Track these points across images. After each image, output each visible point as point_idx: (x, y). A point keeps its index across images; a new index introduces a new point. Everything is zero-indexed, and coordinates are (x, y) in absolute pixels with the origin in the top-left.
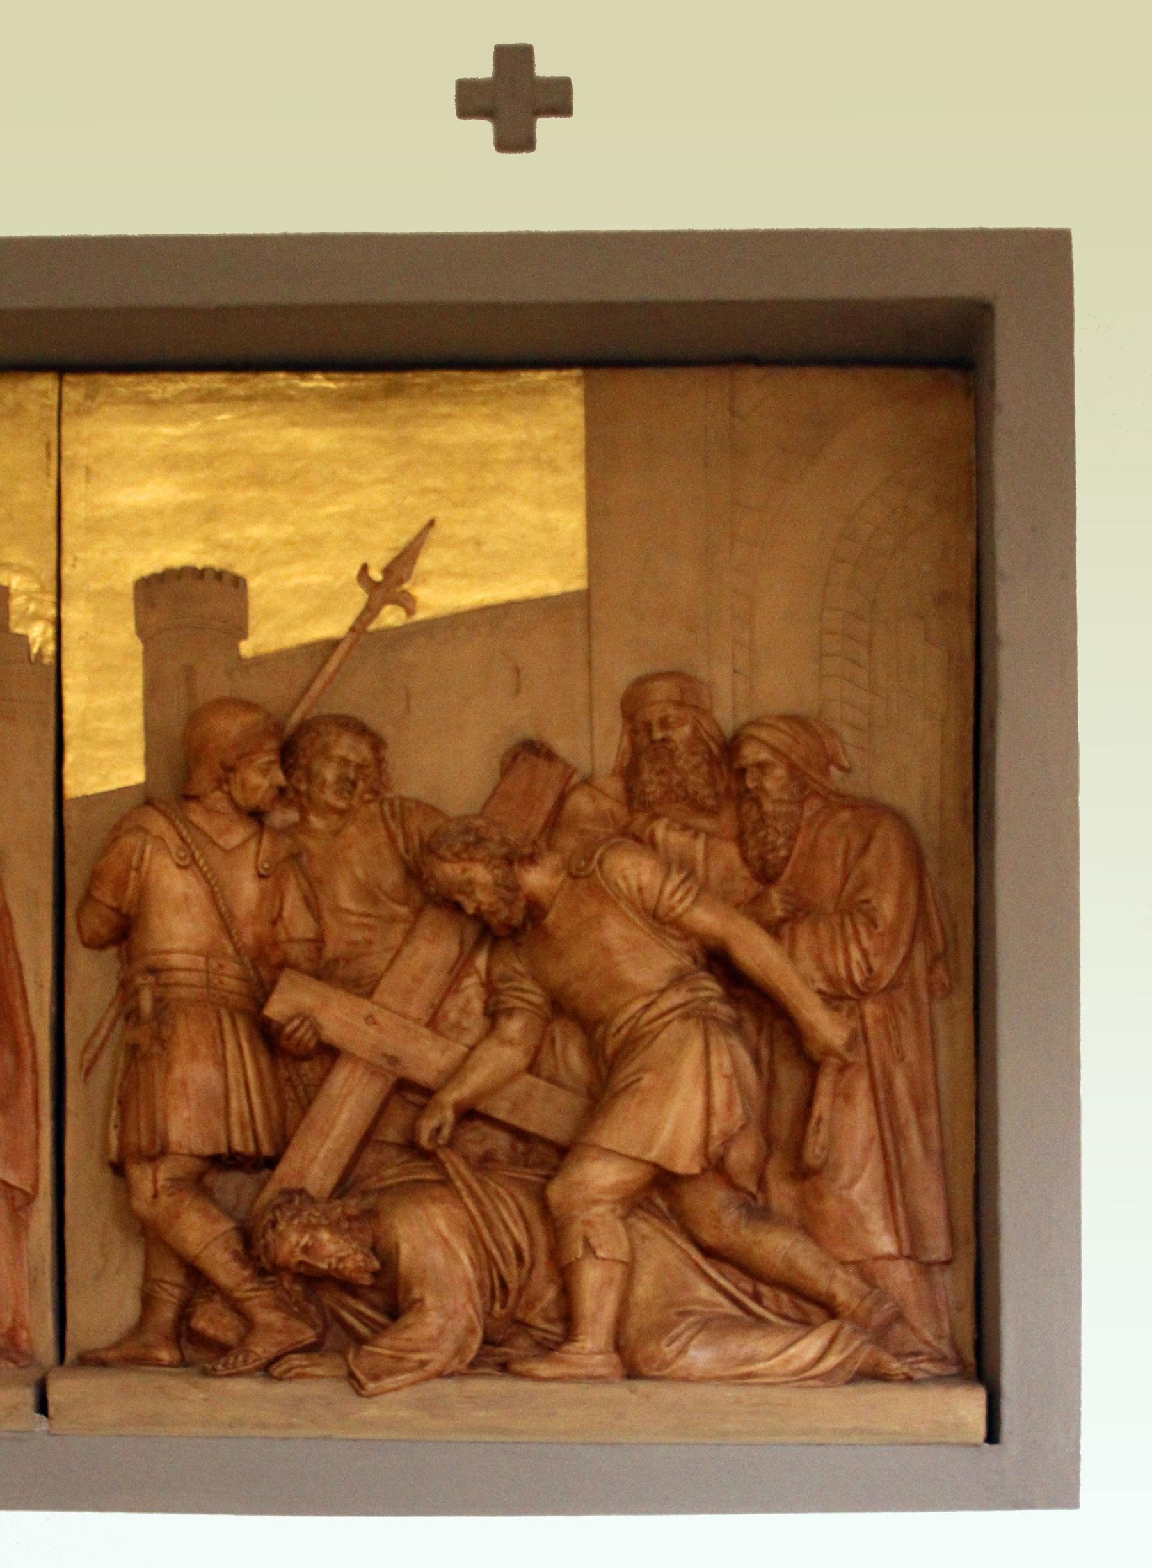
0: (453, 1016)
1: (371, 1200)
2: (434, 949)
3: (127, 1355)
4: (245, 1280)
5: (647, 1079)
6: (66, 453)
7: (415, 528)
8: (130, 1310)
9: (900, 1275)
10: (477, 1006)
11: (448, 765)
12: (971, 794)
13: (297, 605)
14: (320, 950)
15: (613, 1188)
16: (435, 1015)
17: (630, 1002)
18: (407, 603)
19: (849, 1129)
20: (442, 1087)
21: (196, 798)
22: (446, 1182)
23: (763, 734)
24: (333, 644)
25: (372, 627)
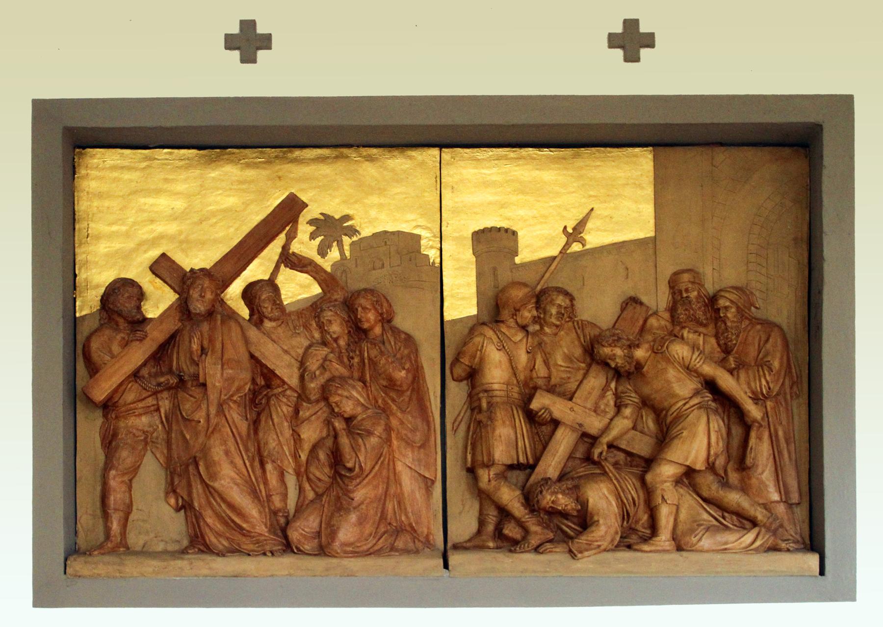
0: (602, 407)
1: (576, 482)
2: (596, 381)
3: (474, 544)
4: (526, 514)
5: (685, 433)
7: (586, 211)
8: (474, 526)
9: (781, 509)
10: (612, 403)
11: (599, 307)
12: (807, 319)
13: (537, 243)
14: (549, 381)
15: (673, 475)
16: (596, 407)
17: (677, 402)
18: (583, 242)
19: (761, 450)
20: (601, 436)
21: (502, 322)
22: (605, 473)
23: (727, 295)
24: (554, 258)
25: (568, 251)
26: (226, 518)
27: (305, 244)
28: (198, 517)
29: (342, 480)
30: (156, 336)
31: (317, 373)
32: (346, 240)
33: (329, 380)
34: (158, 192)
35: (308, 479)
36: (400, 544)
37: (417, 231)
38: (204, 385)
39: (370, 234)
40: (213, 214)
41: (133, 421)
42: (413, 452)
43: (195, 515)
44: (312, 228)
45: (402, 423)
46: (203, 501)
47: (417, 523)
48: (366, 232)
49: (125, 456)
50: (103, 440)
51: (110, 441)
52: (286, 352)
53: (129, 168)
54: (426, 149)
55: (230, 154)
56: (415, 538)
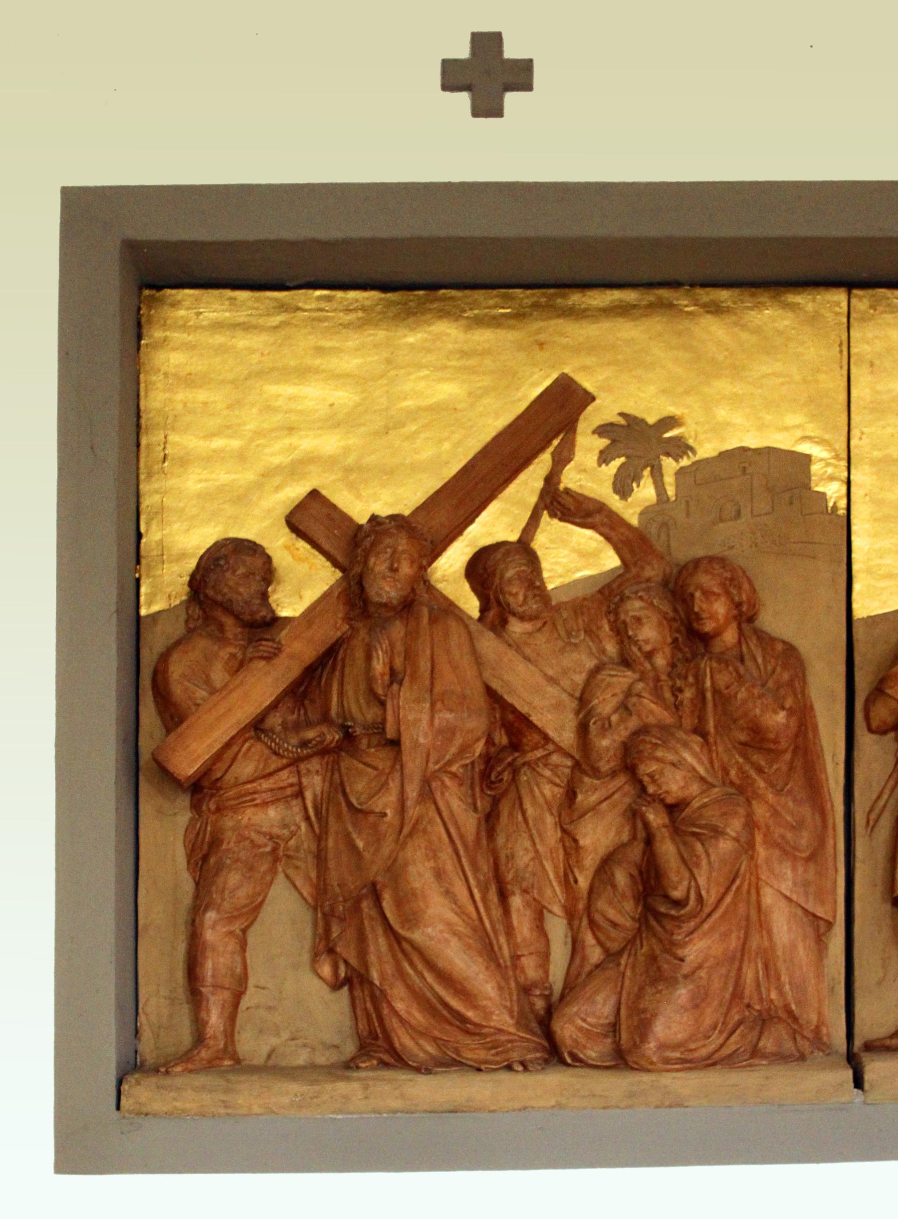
6: (853, 350)
26: (434, 1000)
27: (589, 472)
28: (378, 998)
29: (658, 921)
30: (299, 651)
31: (614, 718)
32: (669, 465)
33: (636, 733)
34: (303, 373)
35: (593, 925)
36: (768, 1044)
37: (804, 448)
38: (395, 744)
39: (714, 454)
40: (412, 415)
41: (250, 816)
42: (794, 869)
43: (373, 998)
44: (604, 442)
45: (776, 813)
46: (389, 969)
47: (798, 1003)
48: (707, 449)
49: (234, 883)
50: (190, 856)
51: (204, 857)
52: (552, 680)
53: (247, 327)
54: (821, 289)
55: (444, 299)
56: (795, 1032)
